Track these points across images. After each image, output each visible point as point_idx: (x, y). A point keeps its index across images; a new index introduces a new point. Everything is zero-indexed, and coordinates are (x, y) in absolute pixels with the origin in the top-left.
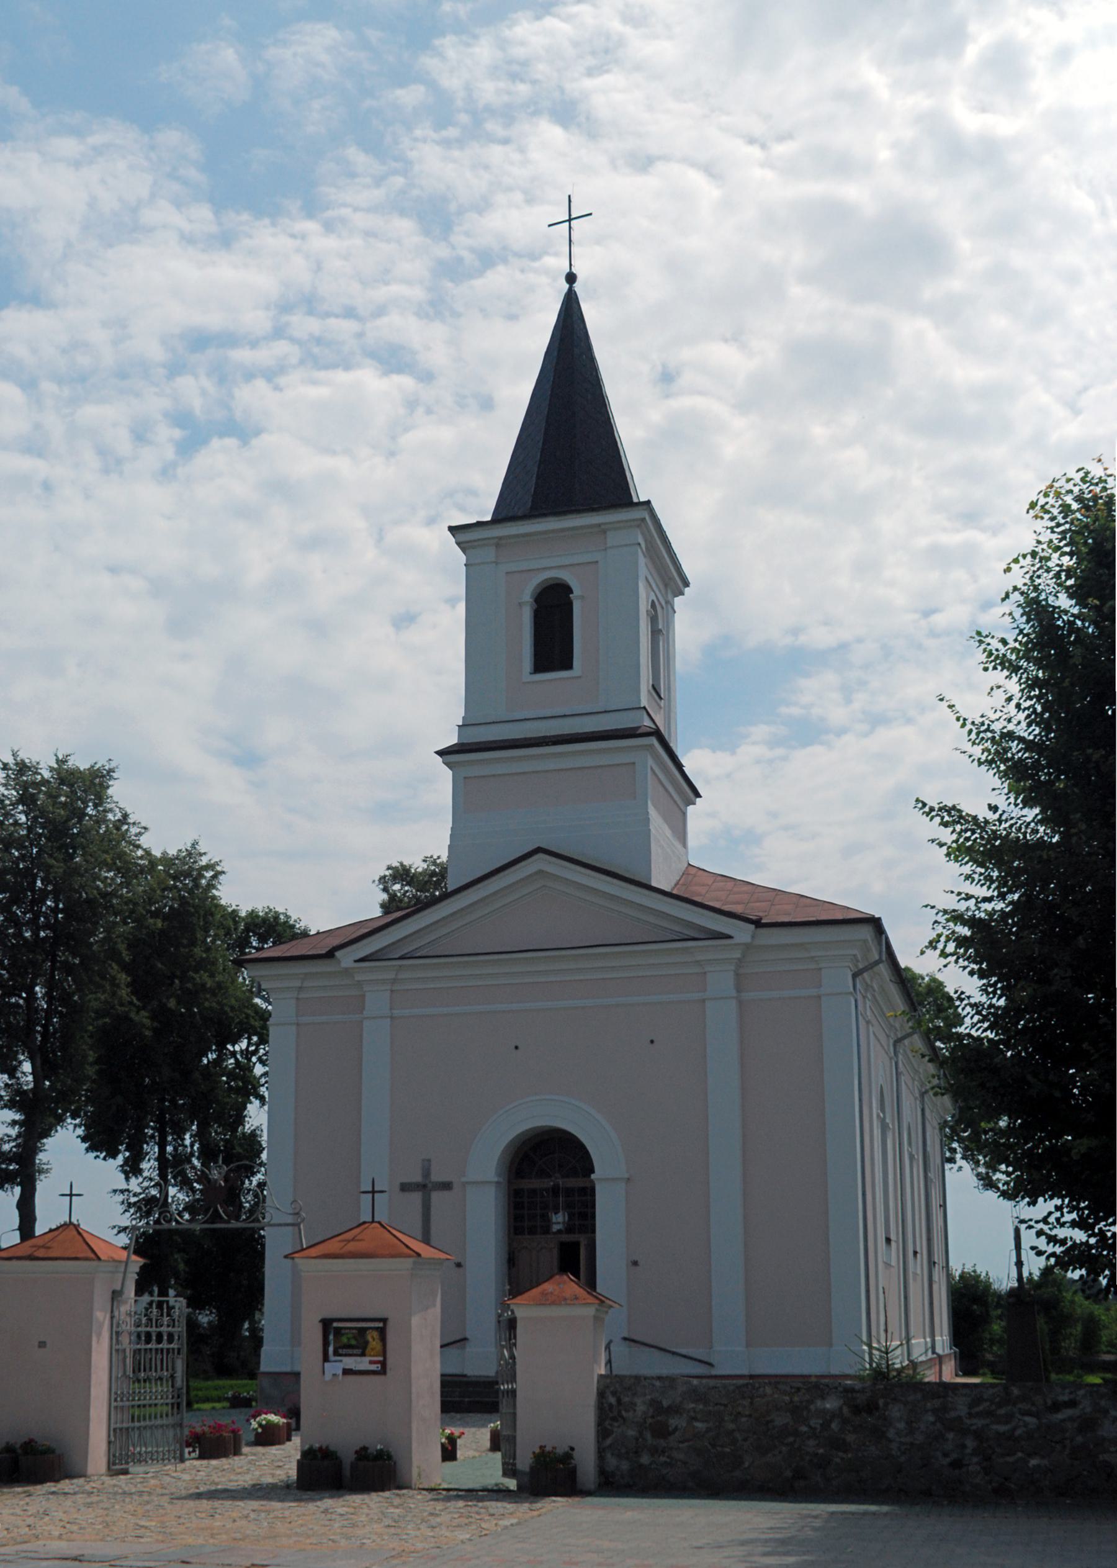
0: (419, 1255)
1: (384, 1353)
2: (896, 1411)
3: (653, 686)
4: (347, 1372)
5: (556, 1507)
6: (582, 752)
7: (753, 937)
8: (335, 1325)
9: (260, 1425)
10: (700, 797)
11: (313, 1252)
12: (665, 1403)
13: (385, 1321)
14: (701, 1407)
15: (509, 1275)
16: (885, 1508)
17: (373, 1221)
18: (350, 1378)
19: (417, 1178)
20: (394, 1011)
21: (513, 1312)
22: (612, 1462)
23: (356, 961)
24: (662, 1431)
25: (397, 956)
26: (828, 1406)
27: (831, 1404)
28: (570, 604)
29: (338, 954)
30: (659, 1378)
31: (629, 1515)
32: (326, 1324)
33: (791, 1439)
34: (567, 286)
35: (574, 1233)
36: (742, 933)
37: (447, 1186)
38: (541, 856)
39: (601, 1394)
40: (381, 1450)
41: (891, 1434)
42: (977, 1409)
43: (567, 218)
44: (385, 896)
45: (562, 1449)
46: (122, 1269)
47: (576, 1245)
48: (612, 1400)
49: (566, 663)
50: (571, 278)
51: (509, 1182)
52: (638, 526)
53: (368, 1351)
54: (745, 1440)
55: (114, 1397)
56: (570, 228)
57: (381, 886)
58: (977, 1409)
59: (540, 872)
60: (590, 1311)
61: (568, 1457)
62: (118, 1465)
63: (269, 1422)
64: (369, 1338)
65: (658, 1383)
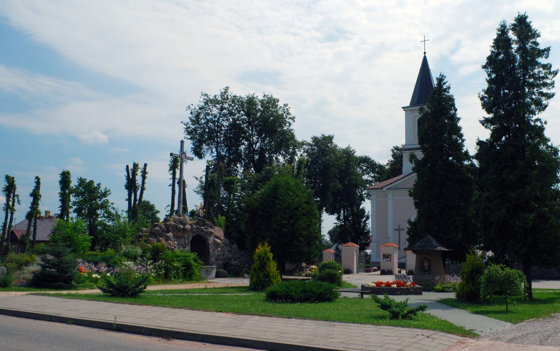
19: (397, 228)
29: (383, 188)
50: (425, 53)
55: (357, 264)
61: (413, 271)
62: (357, 272)
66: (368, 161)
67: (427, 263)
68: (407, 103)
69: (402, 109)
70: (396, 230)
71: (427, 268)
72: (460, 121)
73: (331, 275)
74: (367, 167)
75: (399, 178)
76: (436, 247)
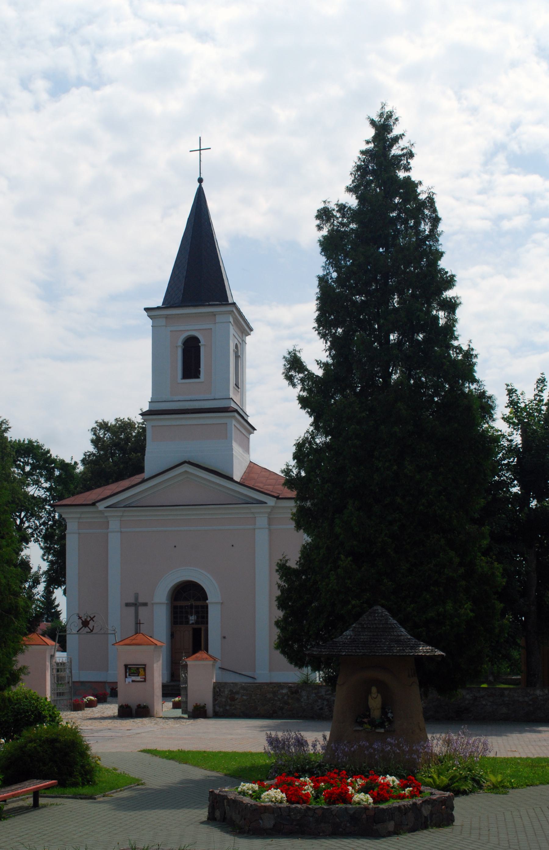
0: (156, 645)
1: (145, 675)
2: (304, 693)
3: (236, 384)
4: (133, 681)
5: (201, 722)
6: (203, 418)
7: (276, 503)
8: (129, 666)
9: (88, 700)
10: (256, 430)
11: (121, 643)
12: (234, 691)
13: (145, 665)
14: (245, 692)
15: (172, 642)
16: (301, 721)
17: (140, 633)
18: (133, 683)
19: (132, 600)
20: (122, 529)
21: (186, 662)
22: (217, 709)
23: (105, 508)
24: (233, 699)
25: (123, 506)
26: (284, 692)
27: (284, 691)
28: (199, 347)
29: (97, 504)
30: (232, 683)
31: (223, 722)
32: (126, 666)
33: (272, 701)
34: (199, 184)
35: (199, 624)
36: (271, 502)
37: (145, 604)
38: (186, 464)
39: (214, 688)
40: (145, 705)
41: (302, 700)
42: (328, 693)
43: (199, 149)
44: (94, 437)
45: (202, 704)
46: (54, 648)
47: (200, 629)
48: (218, 690)
49: (196, 375)
50: (200, 180)
51: (172, 603)
52: (230, 314)
53: (140, 675)
54: (258, 702)
56: (200, 154)
57: (92, 433)
58: (328, 693)
59: (186, 472)
60: (211, 663)
61: (204, 706)
63: (90, 699)
64: (140, 671)
65: (232, 685)
66: (35, 451)
67: (379, 699)
68: (158, 301)
69: (145, 313)
70: (127, 605)
71: (376, 714)
72: (443, 259)
73: (58, 745)
74: (34, 467)
75: (133, 483)
76: (415, 647)
